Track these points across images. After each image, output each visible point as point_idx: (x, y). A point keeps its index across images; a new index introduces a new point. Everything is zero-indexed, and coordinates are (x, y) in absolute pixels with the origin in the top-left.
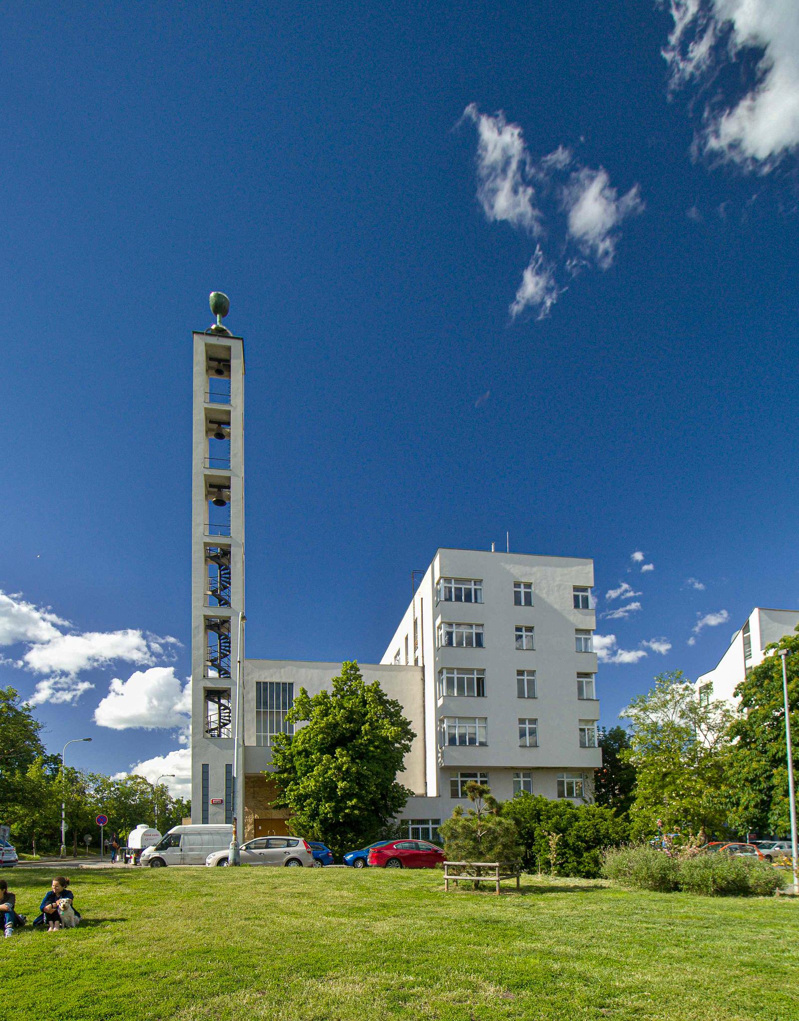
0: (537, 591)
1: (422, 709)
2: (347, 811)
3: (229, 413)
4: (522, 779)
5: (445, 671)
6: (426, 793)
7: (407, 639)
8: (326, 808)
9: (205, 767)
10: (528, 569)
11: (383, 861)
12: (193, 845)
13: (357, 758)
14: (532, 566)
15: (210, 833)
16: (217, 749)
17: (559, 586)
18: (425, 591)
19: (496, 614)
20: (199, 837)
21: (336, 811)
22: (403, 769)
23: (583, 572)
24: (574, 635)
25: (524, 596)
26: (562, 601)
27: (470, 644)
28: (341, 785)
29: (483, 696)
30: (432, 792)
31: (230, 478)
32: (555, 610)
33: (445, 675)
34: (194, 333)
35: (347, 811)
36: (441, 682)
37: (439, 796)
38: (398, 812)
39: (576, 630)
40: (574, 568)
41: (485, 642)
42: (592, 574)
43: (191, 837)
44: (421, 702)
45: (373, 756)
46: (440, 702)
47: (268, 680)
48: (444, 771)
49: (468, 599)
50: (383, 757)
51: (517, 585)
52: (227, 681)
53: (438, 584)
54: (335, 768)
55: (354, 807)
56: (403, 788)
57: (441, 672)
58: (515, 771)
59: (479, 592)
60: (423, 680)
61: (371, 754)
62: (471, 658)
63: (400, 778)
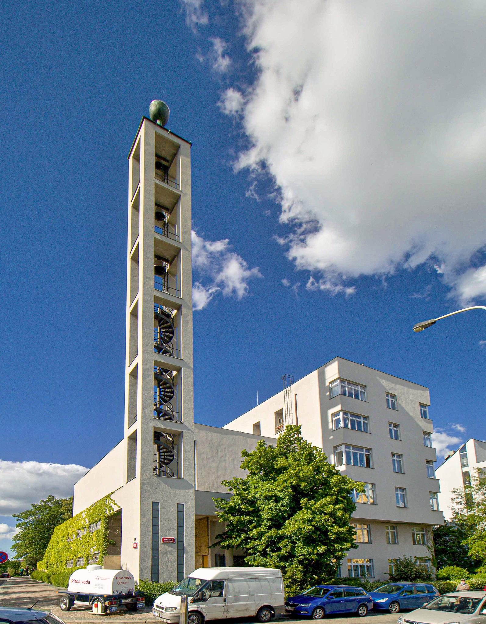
0: (400, 402)
4: (390, 531)
9: (155, 506)
10: (393, 385)
12: (239, 593)
14: (396, 384)
15: (245, 579)
16: (169, 488)
17: (412, 401)
23: (425, 396)
26: (415, 412)
27: (353, 428)
31: (180, 250)
32: (410, 416)
40: (419, 391)
42: (429, 398)
43: (236, 584)
49: (357, 397)
62: (358, 439)
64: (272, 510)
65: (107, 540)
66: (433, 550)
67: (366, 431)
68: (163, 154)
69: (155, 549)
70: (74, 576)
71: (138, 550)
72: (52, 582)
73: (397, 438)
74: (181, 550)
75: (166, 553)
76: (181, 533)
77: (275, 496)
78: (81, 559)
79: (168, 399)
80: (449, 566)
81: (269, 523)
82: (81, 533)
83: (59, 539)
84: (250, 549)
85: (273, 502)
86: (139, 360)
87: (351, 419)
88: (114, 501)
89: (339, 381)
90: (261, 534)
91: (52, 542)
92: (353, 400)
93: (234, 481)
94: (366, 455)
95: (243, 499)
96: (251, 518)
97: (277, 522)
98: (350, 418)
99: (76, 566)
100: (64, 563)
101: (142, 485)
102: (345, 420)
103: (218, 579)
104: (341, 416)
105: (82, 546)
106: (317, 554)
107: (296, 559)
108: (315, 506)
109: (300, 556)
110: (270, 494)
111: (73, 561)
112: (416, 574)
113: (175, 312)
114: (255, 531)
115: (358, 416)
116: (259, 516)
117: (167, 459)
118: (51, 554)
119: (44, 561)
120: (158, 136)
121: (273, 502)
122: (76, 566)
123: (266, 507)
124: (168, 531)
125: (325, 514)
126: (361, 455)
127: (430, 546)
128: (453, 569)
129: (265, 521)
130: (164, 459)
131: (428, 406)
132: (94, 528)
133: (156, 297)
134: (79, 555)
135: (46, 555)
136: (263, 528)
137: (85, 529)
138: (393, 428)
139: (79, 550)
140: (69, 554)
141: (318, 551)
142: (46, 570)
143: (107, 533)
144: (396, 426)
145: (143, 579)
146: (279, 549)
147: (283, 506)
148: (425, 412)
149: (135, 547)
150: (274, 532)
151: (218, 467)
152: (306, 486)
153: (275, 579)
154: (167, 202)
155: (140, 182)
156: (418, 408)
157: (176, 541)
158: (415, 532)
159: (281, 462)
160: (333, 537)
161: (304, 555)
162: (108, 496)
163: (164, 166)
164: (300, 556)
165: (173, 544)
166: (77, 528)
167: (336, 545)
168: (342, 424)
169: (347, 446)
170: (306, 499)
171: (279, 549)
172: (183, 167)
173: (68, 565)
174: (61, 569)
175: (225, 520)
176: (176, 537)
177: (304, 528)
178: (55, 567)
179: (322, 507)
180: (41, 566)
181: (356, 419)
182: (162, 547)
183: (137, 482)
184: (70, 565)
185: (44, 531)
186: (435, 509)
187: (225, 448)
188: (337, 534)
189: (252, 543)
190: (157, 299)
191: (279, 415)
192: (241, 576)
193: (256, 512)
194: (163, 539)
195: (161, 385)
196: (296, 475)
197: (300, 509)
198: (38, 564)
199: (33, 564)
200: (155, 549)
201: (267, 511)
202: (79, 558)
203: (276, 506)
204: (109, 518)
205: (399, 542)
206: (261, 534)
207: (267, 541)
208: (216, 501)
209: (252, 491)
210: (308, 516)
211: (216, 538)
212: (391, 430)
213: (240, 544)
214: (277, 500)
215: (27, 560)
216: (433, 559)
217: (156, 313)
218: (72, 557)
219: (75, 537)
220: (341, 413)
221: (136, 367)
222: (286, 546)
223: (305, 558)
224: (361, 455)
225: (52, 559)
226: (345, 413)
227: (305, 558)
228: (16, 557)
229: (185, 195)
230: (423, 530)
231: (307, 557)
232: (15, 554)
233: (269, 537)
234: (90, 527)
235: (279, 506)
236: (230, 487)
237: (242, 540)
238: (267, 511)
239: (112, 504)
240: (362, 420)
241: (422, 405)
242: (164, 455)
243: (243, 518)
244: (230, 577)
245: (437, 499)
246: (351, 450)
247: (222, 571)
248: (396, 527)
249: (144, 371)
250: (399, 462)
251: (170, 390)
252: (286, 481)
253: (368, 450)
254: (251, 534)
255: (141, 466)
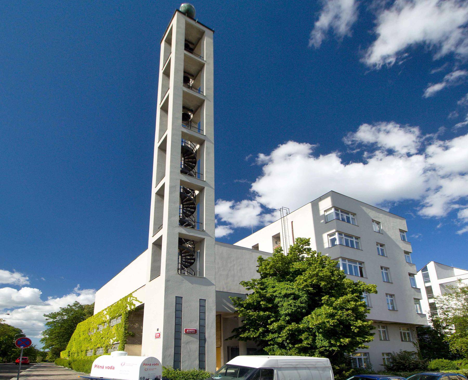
4: (381, 329)
9: (179, 300)
27: (347, 245)
31: (204, 101)
43: (286, 372)
49: (348, 221)
64: (291, 306)
65: (126, 332)
66: (418, 346)
67: (358, 248)
68: (191, 38)
69: (178, 339)
70: (97, 362)
71: (161, 340)
72: (73, 367)
73: (383, 255)
74: (202, 340)
75: (188, 343)
76: (202, 326)
77: (293, 294)
78: (100, 349)
79: (190, 214)
80: (439, 359)
81: (287, 318)
82: (101, 328)
83: (81, 333)
84: (270, 340)
85: (291, 299)
86: (166, 180)
87: (345, 239)
88: (136, 298)
89: (333, 209)
90: (281, 328)
91: (74, 335)
92: (345, 224)
93: (251, 282)
94: (360, 267)
95: (261, 296)
96: (270, 313)
97: (296, 317)
98: (344, 237)
99: (95, 354)
100: (84, 352)
101: (167, 281)
102: (340, 239)
103: (268, 366)
104: (336, 236)
105: (102, 338)
106: (340, 346)
107: (317, 350)
108: (336, 302)
109: (320, 348)
110: (289, 292)
111: (93, 350)
112: (414, 366)
113: (198, 147)
114: (275, 325)
115: (351, 236)
116: (277, 312)
117: (188, 263)
118: (73, 345)
119: (67, 350)
120: (187, 24)
121: (291, 299)
122: (95, 354)
123: (285, 304)
124: (190, 322)
125: (347, 310)
126: (355, 267)
127: (415, 342)
128: (442, 361)
129: (283, 317)
130: (185, 262)
131: (406, 232)
132: (114, 322)
133: (183, 133)
134: (99, 345)
135: (69, 345)
136: (281, 322)
137: (106, 324)
138: (380, 247)
139: (99, 342)
140: (89, 345)
141: (341, 343)
142: (68, 358)
143: (127, 325)
144: (382, 245)
145: (166, 367)
146: (301, 341)
147: (301, 303)
148: (404, 236)
149: (158, 337)
150: (293, 326)
151: (227, 275)
152: (325, 285)
153: (324, 369)
154: (193, 70)
155: (171, 56)
156: (398, 233)
157: (198, 332)
158: (402, 331)
159: (297, 266)
160: (356, 331)
161: (325, 347)
162: (130, 295)
163: (191, 46)
164: (320, 348)
165: (195, 335)
166: (98, 323)
167: (358, 338)
168: (337, 242)
169: (344, 259)
170: (328, 296)
171: (301, 341)
172: (207, 46)
173: (88, 354)
174: (82, 356)
175: (244, 315)
176: (198, 328)
177: (328, 322)
178: (76, 355)
179: (345, 303)
180: (63, 355)
181: (349, 239)
182: (184, 338)
183: (161, 280)
184: (90, 354)
185: (68, 329)
186: (419, 312)
187: (234, 260)
188: (359, 327)
189: (270, 336)
190: (184, 134)
191: (277, 238)
192: (291, 365)
193: (275, 309)
194: (186, 330)
195: (184, 202)
196: (317, 275)
197: (320, 306)
198: (61, 353)
199: (57, 354)
200: (178, 339)
201: (286, 307)
202: (99, 348)
203: (294, 303)
204: (130, 312)
205: (390, 339)
206: (281, 328)
207: (288, 334)
208: (233, 300)
209: (270, 290)
210: (331, 310)
211: (233, 332)
212: (378, 248)
213: (259, 337)
214: (296, 297)
215: (52, 350)
216: (419, 353)
217: (182, 146)
218: (92, 347)
219: (95, 331)
220: (337, 233)
221: (163, 186)
222: (307, 339)
223: (325, 350)
224: (355, 267)
225: (74, 349)
226: (340, 234)
227: (325, 350)
228: (43, 348)
229: (208, 64)
230: (408, 330)
231: (327, 348)
232: (43, 345)
233: (289, 330)
234: (110, 322)
235: (298, 303)
236: (248, 287)
237: (260, 333)
238: (286, 307)
239: (133, 301)
240: (354, 240)
241: (401, 231)
242: (185, 259)
243: (262, 313)
244: (280, 365)
245: (419, 304)
246: (347, 263)
247: (269, 359)
248: (386, 326)
249: (171, 187)
250: (387, 274)
251: (192, 206)
252: (306, 281)
253: (361, 263)
254: (271, 327)
255: (166, 265)
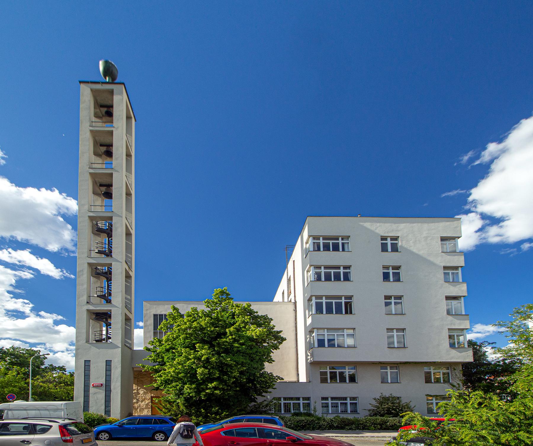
1: (294, 328)
2: (208, 391)
3: (111, 133)
4: (389, 371)
5: (314, 298)
6: (298, 380)
7: (283, 293)
8: (187, 389)
9: (87, 363)
11: (489, 332)
13: (222, 353)
17: (426, 238)
18: (297, 255)
19: (364, 262)
20: (25, 412)
21: (198, 391)
22: (271, 361)
24: (442, 271)
25: (390, 245)
28: (199, 371)
29: (351, 313)
30: (303, 379)
33: (314, 301)
34: (80, 82)
35: (208, 391)
36: (310, 309)
37: (309, 381)
38: (267, 392)
39: (387, 329)
41: (352, 277)
43: (15, 412)
44: (293, 324)
45: (238, 351)
46: (309, 321)
47: (163, 313)
48: (312, 365)
50: (248, 351)
51: (384, 238)
52: (109, 305)
53: (307, 243)
54: (194, 358)
55: (215, 388)
56: (272, 375)
57: (310, 300)
58: (383, 365)
59: (346, 246)
60: (295, 310)
61: (235, 349)
63: (268, 368)
